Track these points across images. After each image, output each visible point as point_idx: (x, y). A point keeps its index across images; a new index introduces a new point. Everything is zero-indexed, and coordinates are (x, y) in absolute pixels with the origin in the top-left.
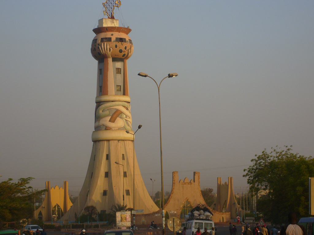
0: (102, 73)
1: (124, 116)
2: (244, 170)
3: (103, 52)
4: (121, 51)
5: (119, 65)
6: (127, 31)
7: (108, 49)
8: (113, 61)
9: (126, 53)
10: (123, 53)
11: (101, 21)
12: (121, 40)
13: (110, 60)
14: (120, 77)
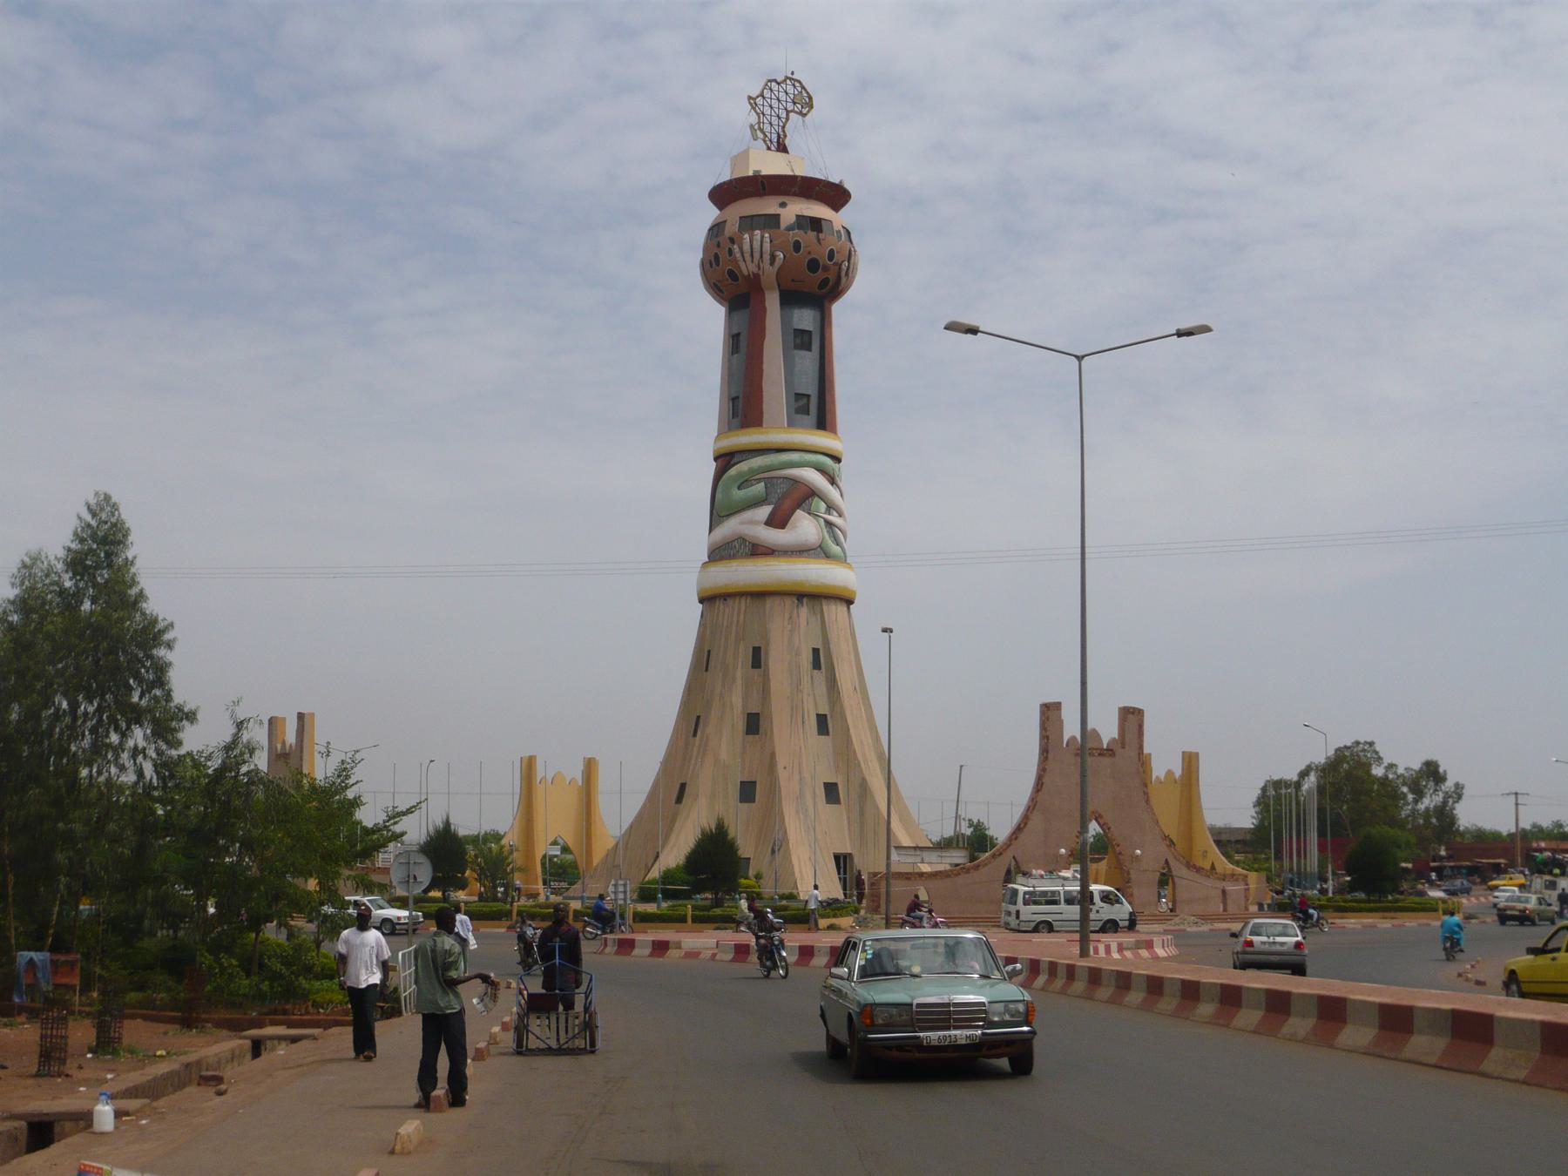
0: (744, 350)
1: (823, 506)
2: (555, 843)
3: (747, 268)
4: (813, 265)
5: (805, 318)
6: (836, 195)
7: (767, 257)
8: (782, 303)
9: (832, 278)
10: (820, 275)
11: (744, 156)
12: (816, 224)
13: (772, 301)
14: (807, 361)
